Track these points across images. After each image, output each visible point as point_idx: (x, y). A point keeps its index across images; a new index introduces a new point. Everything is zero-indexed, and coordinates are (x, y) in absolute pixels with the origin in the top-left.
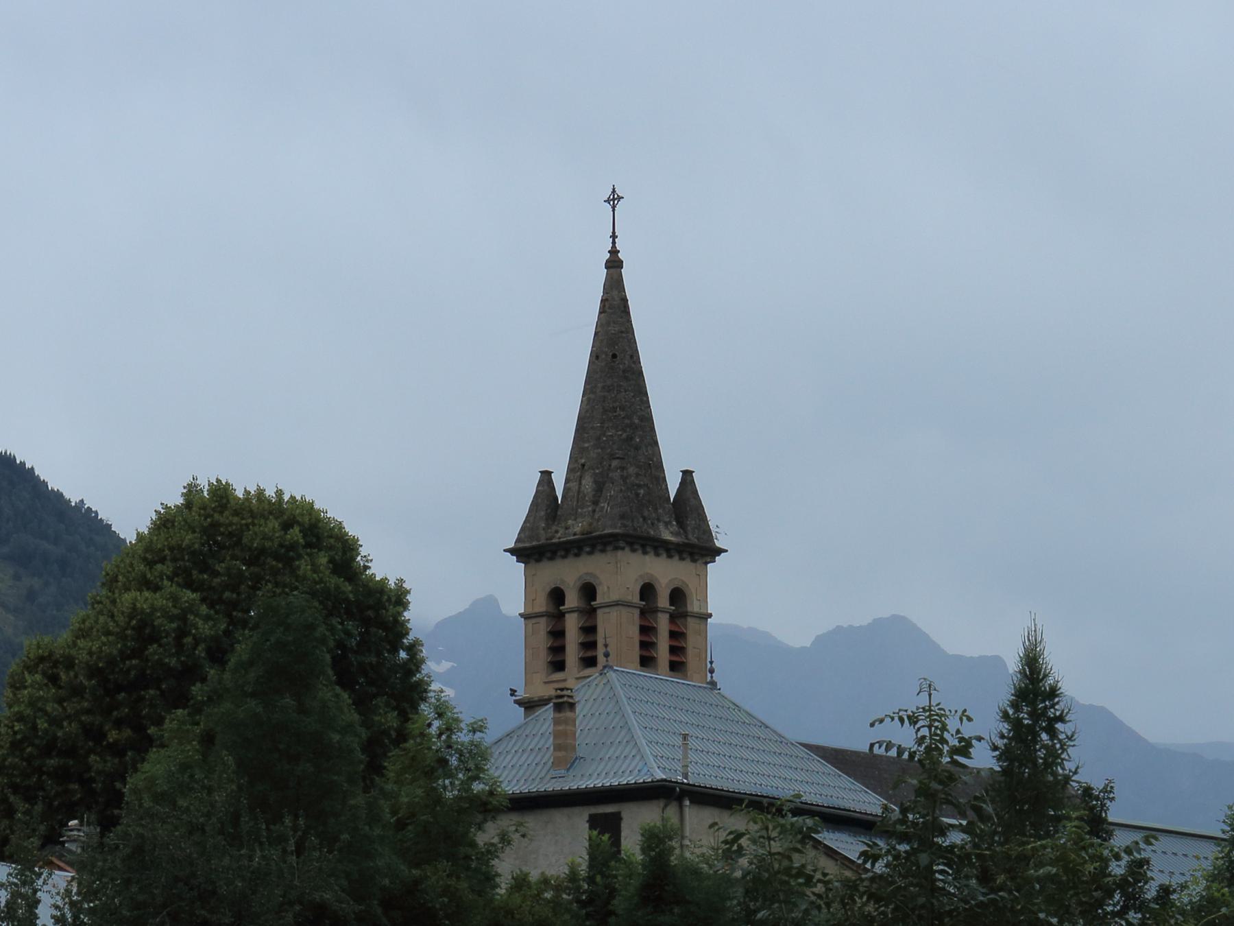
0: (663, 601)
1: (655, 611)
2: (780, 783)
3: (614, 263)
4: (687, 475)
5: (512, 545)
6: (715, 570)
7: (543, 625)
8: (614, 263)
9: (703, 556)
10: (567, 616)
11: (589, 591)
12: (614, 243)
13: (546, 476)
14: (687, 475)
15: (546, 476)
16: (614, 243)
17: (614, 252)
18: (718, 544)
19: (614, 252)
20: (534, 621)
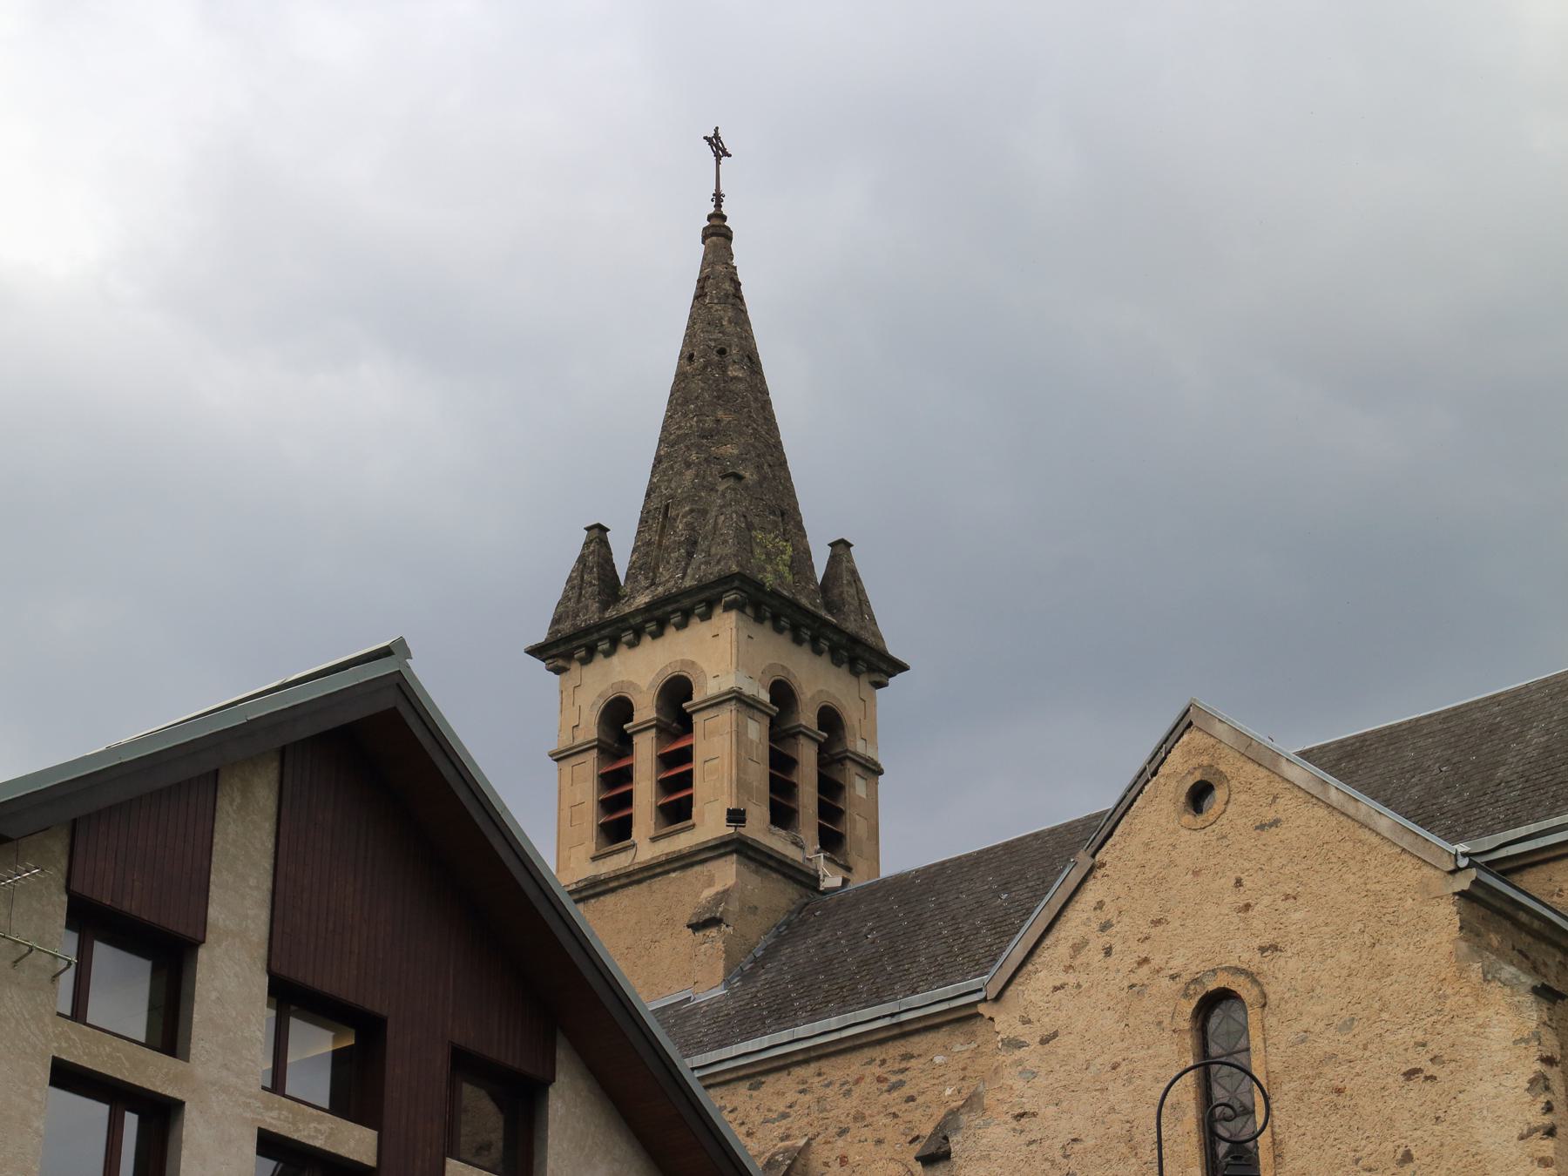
0: (807, 717)
1: (796, 734)
2: (1045, 912)
3: (717, 232)
4: (841, 548)
5: (540, 636)
6: (893, 696)
7: (589, 765)
8: (717, 232)
9: (872, 669)
10: (636, 739)
11: (676, 691)
12: (718, 206)
13: (598, 534)
14: (841, 548)
15: (598, 534)
16: (718, 206)
17: (718, 217)
18: (893, 650)
19: (718, 217)
20: (574, 760)
